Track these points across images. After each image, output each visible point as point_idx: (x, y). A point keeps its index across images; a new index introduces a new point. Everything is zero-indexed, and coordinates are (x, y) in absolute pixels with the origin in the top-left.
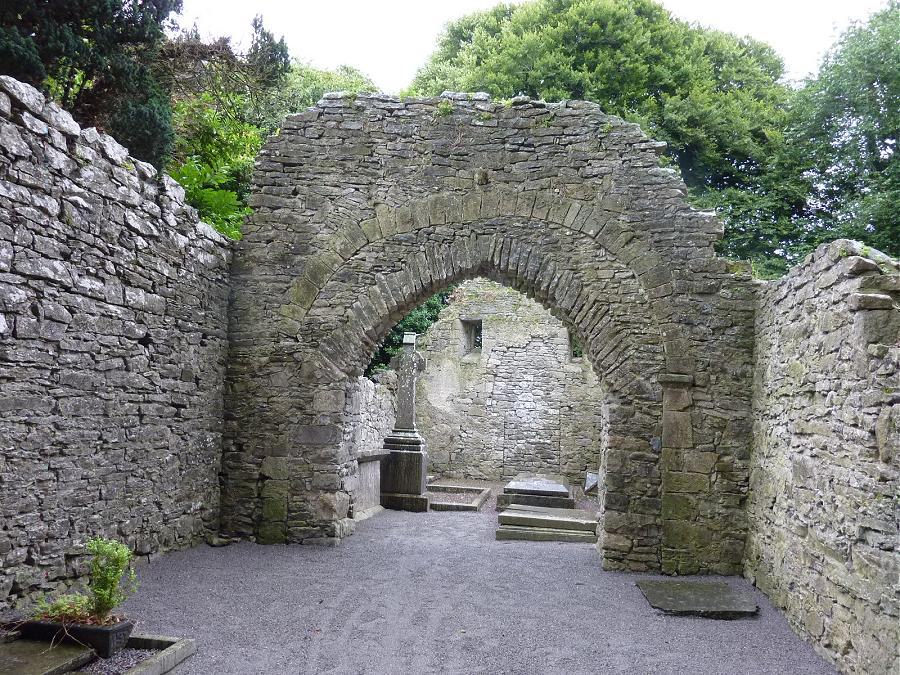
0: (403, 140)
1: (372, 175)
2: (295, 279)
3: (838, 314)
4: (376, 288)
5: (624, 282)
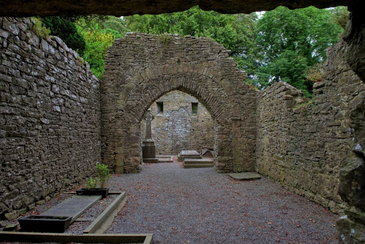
1: (144, 59)
2: (121, 92)
3: (280, 100)
4: (147, 94)
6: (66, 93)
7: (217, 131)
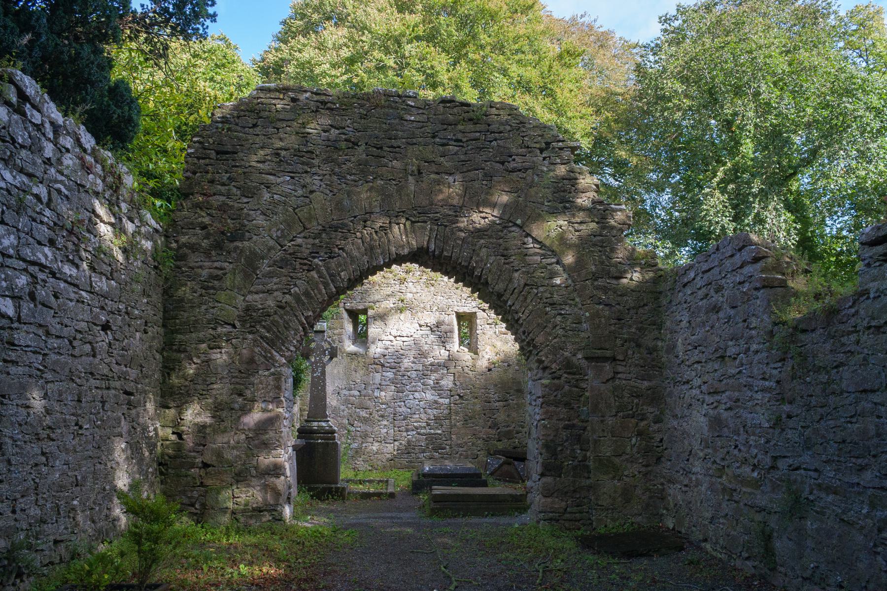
0: (337, 132)
4: (314, 274)
5: (549, 267)
6: (40, 256)
7: (540, 395)
